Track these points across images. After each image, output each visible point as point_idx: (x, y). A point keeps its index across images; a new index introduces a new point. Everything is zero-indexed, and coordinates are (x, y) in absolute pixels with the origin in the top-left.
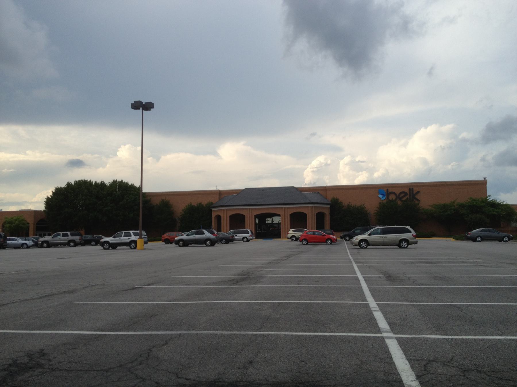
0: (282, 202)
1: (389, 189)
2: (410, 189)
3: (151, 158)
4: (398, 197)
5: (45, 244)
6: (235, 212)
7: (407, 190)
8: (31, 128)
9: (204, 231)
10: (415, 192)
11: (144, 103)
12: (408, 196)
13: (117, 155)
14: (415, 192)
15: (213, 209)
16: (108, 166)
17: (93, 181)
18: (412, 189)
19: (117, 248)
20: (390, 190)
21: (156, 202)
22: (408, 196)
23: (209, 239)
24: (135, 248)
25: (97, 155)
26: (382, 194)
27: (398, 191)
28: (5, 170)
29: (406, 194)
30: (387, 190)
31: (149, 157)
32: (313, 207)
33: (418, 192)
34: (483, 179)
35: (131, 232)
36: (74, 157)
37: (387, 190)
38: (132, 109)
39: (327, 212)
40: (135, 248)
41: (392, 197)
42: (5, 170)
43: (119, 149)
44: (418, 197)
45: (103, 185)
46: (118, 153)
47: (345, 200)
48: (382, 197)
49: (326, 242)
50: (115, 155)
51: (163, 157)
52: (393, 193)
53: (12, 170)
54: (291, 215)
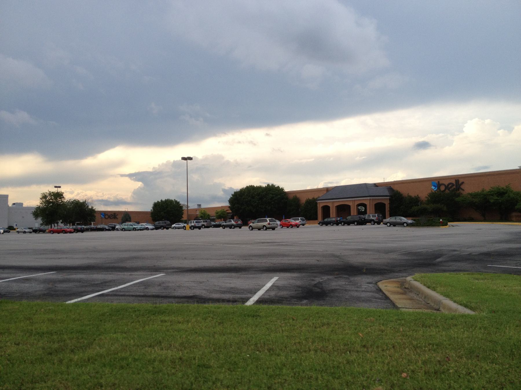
0: (330, 198)
1: (440, 181)
2: (456, 180)
3: (502, 130)
4: (447, 187)
5: (203, 227)
6: (378, 202)
7: (453, 182)
8: (377, 116)
9: (232, 220)
10: (460, 182)
11: (10, 204)
12: (455, 187)
13: (464, 132)
14: (460, 182)
15: (319, 201)
16: (454, 144)
17: (255, 186)
18: (458, 180)
19: (352, 279)
20: (441, 182)
21: (291, 197)
22: (455, 187)
23: (233, 225)
24: (186, 229)
25: (441, 135)
26: (434, 186)
27: (446, 183)
28: (358, 158)
29: (453, 185)
30: (439, 182)
31: (499, 129)
32: (371, 199)
33: (463, 183)
34: (519, 168)
35: (300, 218)
36: (421, 140)
37: (439, 182)
38: (22, 202)
39: (387, 203)
40: (186, 229)
41: (442, 188)
42: (358, 158)
43: (465, 125)
44: (462, 187)
45: (259, 188)
46: (464, 129)
47: (404, 191)
48: (435, 188)
49: (403, 225)
50: (462, 131)
51: (516, 128)
52: (443, 184)
53: (364, 157)
54: (375, 205)
